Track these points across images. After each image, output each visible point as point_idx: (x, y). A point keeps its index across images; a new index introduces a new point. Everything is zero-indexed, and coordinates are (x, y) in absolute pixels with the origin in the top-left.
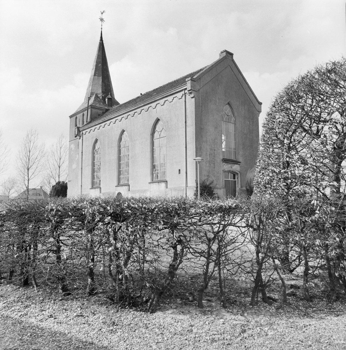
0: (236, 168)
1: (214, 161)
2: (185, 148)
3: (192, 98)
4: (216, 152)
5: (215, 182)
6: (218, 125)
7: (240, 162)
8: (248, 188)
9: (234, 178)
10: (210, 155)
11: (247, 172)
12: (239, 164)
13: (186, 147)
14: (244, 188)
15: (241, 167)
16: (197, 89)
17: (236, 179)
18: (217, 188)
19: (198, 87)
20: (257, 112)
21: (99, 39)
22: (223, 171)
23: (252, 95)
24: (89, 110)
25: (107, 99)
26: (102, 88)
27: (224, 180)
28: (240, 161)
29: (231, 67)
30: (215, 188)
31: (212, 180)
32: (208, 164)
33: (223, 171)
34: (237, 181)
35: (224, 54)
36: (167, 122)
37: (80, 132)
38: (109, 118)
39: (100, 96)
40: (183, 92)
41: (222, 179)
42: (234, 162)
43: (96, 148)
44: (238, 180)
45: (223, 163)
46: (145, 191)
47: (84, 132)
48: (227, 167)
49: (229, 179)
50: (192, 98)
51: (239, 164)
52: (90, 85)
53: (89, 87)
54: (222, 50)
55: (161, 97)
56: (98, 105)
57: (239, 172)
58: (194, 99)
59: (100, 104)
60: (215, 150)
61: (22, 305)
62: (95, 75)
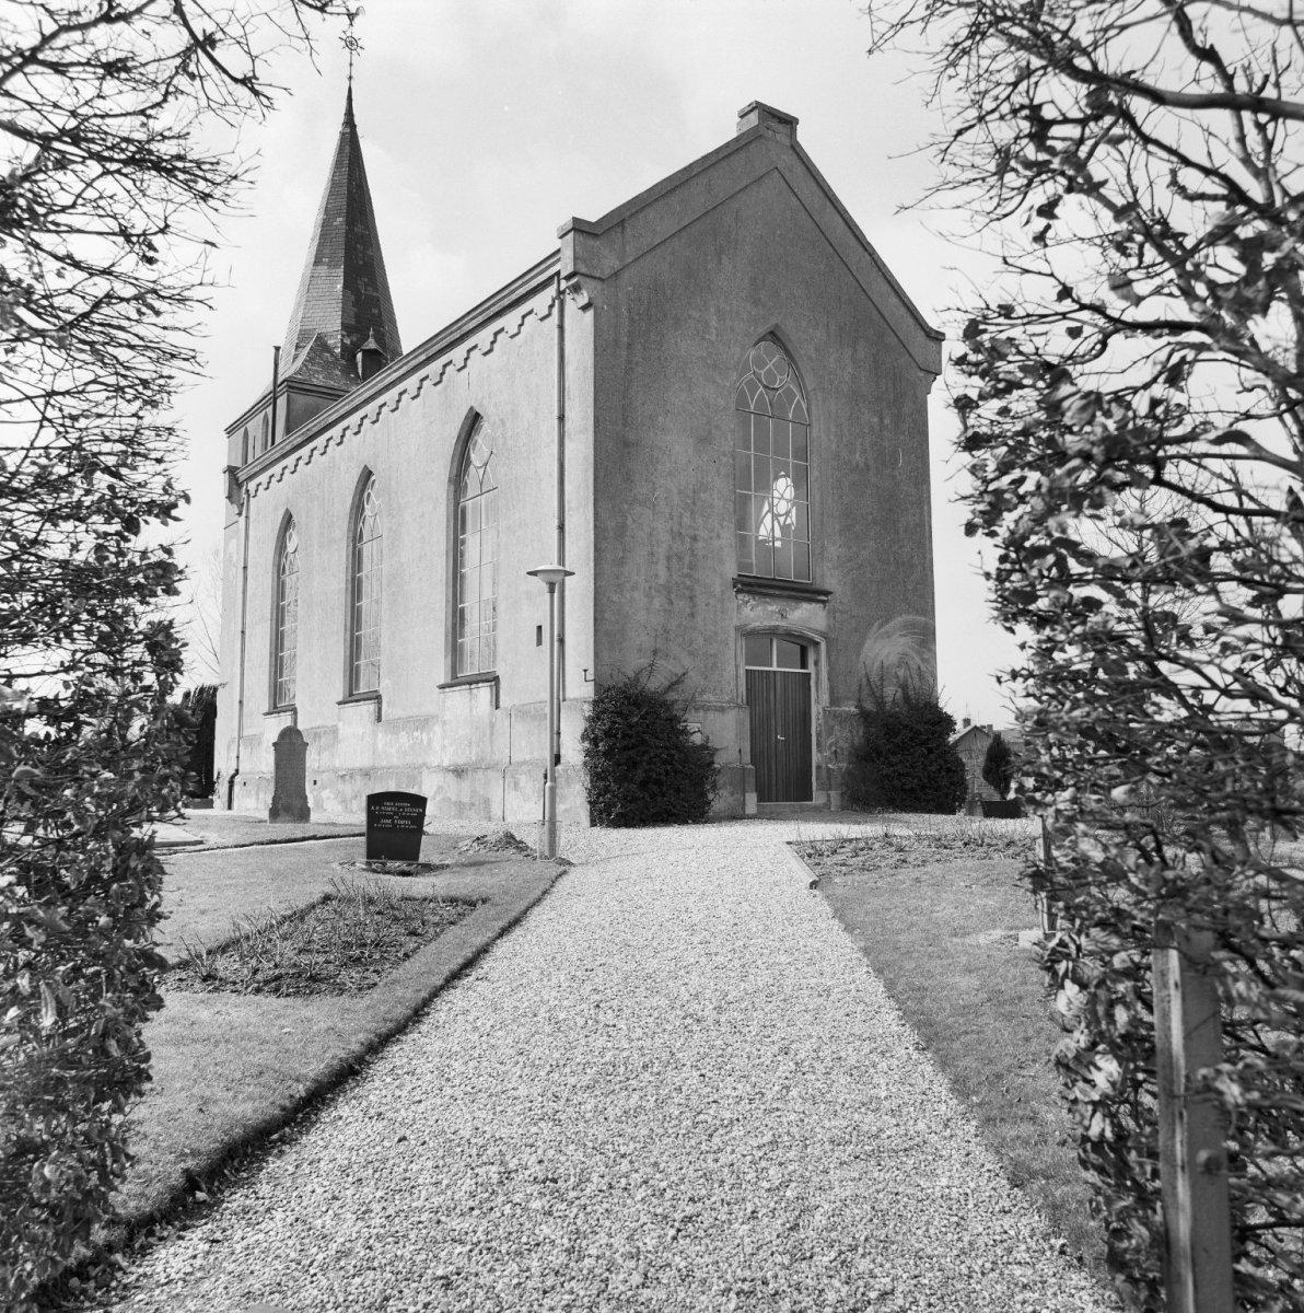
0: (806, 616)
1: (690, 589)
2: (555, 533)
3: (585, 308)
4: (700, 545)
5: (694, 679)
6: (717, 427)
7: (827, 593)
8: (869, 706)
9: (804, 665)
10: (668, 559)
11: (864, 638)
12: (823, 602)
13: (561, 528)
14: (850, 708)
15: (832, 614)
16: (608, 272)
17: (811, 669)
18: (706, 708)
19: (610, 263)
20: (921, 374)
21: (342, 118)
22: (737, 629)
23: (894, 300)
24: (282, 402)
25: (359, 356)
26: (344, 311)
27: (742, 672)
28: (827, 587)
29: (787, 175)
30: (690, 704)
31: (680, 671)
32: (657, 603)
33: (737, 629)
34: (813, 676)
35: (754, 118)
36: (503, 422)
37: (240, 486)
38: (323, 425)
39: (335, 342)
40: (551, 291)
41: (731, 668)
42: (793, 589)
43: (290, 548)
44: (819, 670)
45: (740, 596)
46: (426, 720)
47: (252, 486)
48: (760, 613)
49: (775, 668)
50: (585, 308)
51: (823, 602)
52: (299, 304)
53: (296, 311)
54: (744, 103)
55: (480, 319)
56: (319, 380)
57: (823, 635)
58: (590, 314)
59: (329, 376)
60: (695, 538)
61: (812, 1024)
62: (317, 262)
